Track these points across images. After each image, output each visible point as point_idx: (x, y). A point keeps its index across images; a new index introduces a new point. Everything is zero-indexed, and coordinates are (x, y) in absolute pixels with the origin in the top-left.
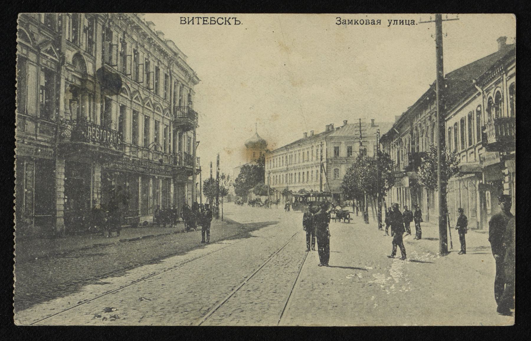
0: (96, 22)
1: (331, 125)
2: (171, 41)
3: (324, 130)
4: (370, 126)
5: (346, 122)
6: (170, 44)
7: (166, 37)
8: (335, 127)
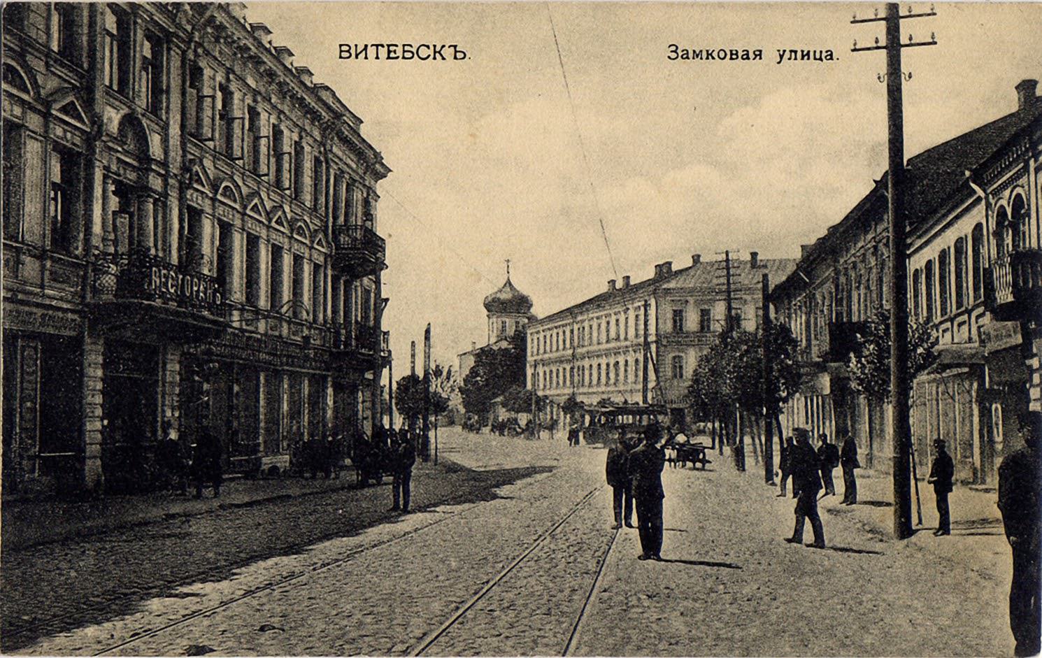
0: (169, 49)
1: (667, 263)
2: (327, 88)
3: (650, 274)
4: (749, 265)
5: (696, 259)
6: (325, 95)
7: (298, 61)
8: (675, 268)
